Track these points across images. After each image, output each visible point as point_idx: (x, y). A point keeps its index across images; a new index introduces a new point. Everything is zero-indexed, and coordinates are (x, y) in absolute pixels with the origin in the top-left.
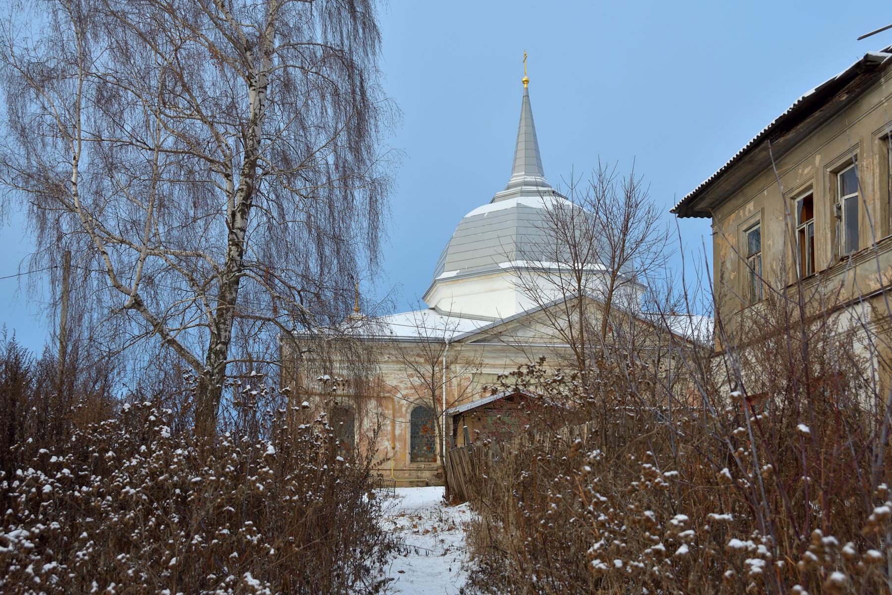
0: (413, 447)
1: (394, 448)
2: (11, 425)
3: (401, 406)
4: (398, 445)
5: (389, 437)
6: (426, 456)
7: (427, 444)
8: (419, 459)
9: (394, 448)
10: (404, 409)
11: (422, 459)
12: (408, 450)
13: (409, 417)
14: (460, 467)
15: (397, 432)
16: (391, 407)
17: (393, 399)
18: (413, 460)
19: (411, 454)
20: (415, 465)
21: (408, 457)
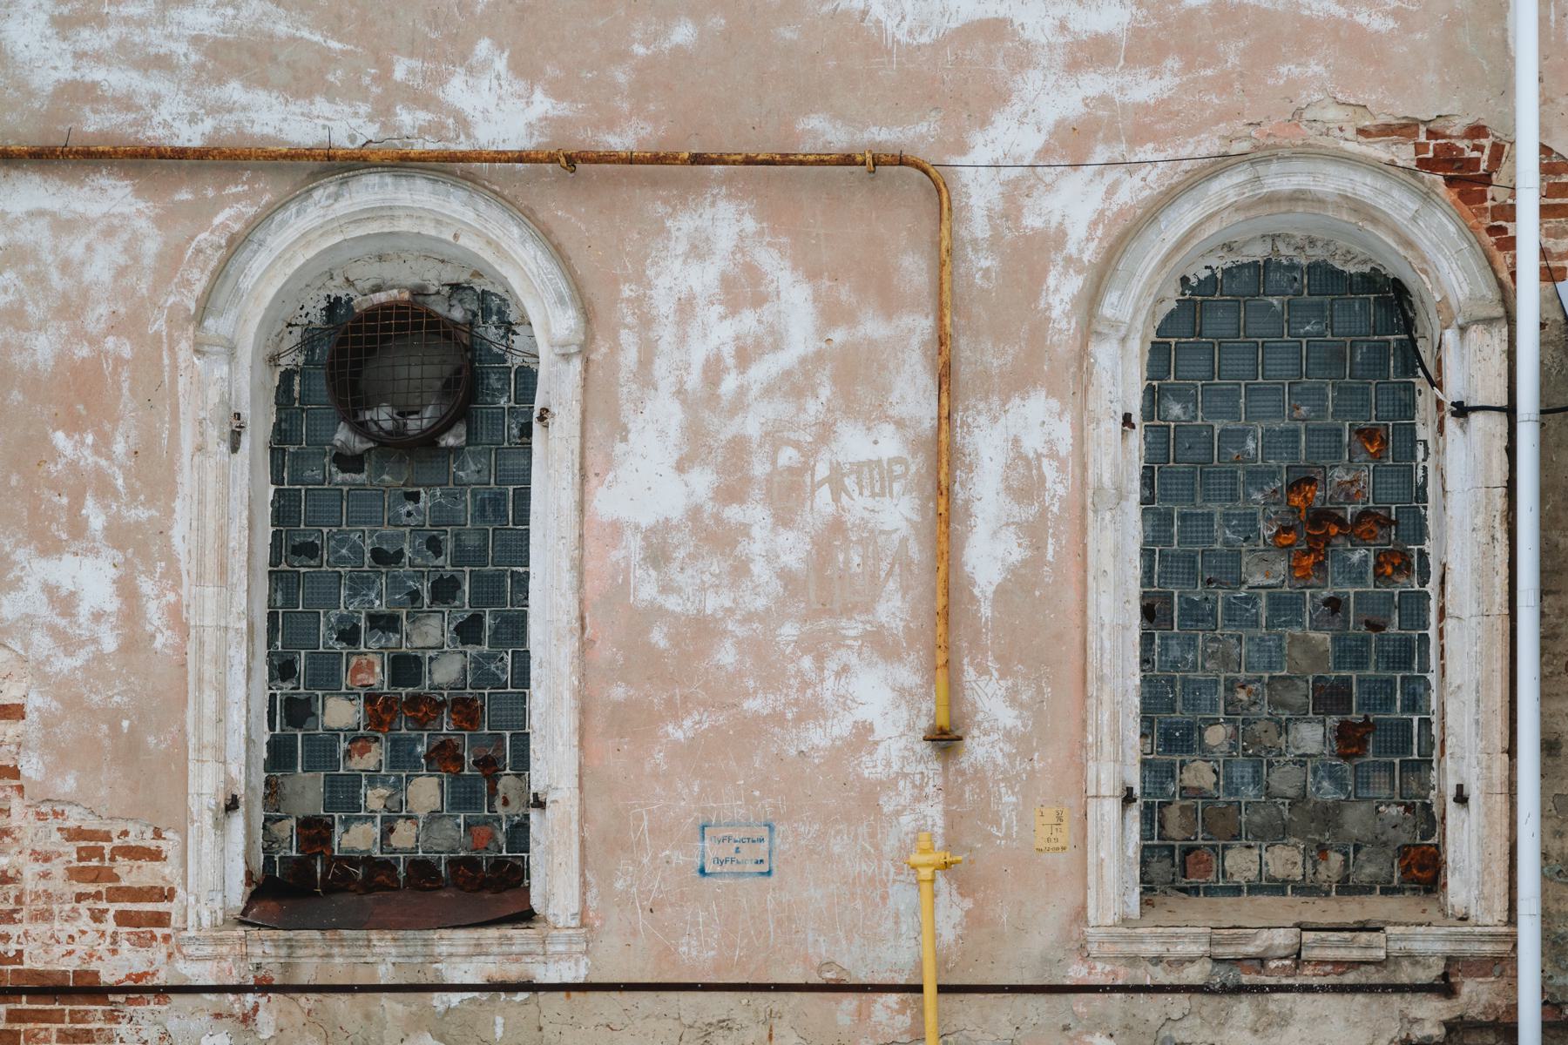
0: (1168, 728)
1: (945, 739)
2: (177, 586)
3: (1032, 254)
4: (992, 702)
5: (893, 609)
6: (1316, 824)
7: (1330, 697)
8: (1240, 863)
9: (945, 739)
10: (1062, 292)
11: (1283, 860)
12: (1116, 753)
13: (1121, 375)
14: (210, 697)
15: (988, 556)
16: (914, 270)
17: (936, 185)
18: (1175, 864)
19: (1152, 802)
20: (1187, 937)
21: (1115, 841)
